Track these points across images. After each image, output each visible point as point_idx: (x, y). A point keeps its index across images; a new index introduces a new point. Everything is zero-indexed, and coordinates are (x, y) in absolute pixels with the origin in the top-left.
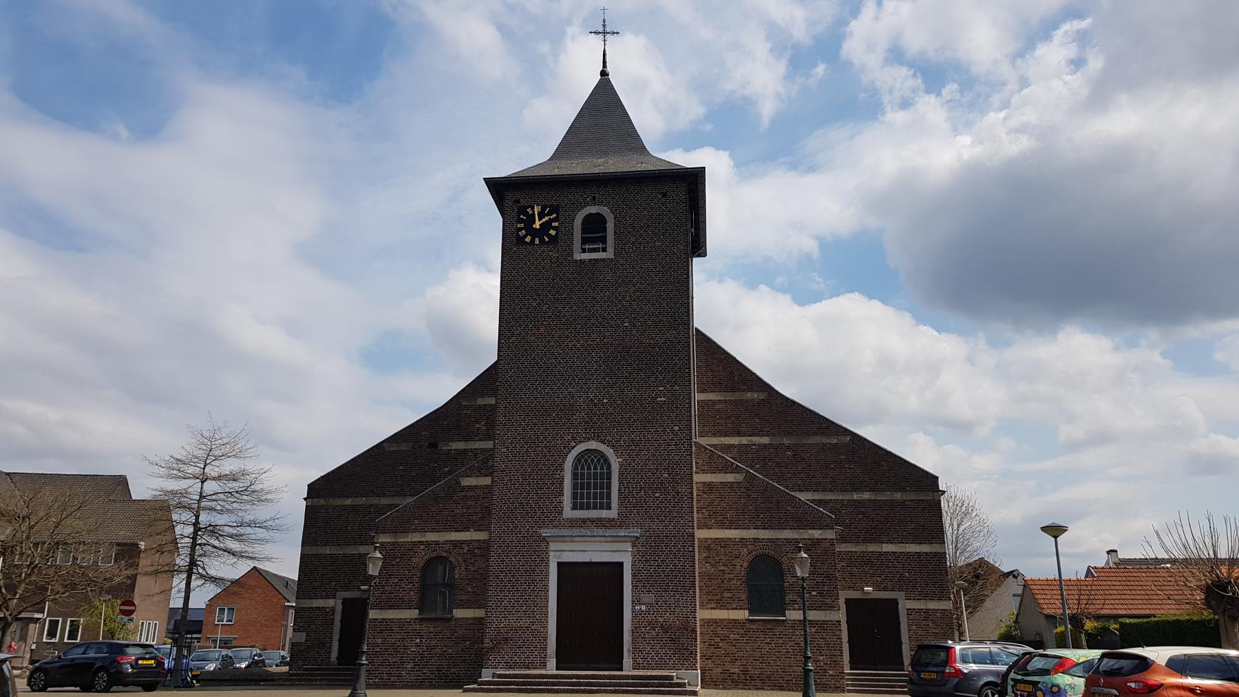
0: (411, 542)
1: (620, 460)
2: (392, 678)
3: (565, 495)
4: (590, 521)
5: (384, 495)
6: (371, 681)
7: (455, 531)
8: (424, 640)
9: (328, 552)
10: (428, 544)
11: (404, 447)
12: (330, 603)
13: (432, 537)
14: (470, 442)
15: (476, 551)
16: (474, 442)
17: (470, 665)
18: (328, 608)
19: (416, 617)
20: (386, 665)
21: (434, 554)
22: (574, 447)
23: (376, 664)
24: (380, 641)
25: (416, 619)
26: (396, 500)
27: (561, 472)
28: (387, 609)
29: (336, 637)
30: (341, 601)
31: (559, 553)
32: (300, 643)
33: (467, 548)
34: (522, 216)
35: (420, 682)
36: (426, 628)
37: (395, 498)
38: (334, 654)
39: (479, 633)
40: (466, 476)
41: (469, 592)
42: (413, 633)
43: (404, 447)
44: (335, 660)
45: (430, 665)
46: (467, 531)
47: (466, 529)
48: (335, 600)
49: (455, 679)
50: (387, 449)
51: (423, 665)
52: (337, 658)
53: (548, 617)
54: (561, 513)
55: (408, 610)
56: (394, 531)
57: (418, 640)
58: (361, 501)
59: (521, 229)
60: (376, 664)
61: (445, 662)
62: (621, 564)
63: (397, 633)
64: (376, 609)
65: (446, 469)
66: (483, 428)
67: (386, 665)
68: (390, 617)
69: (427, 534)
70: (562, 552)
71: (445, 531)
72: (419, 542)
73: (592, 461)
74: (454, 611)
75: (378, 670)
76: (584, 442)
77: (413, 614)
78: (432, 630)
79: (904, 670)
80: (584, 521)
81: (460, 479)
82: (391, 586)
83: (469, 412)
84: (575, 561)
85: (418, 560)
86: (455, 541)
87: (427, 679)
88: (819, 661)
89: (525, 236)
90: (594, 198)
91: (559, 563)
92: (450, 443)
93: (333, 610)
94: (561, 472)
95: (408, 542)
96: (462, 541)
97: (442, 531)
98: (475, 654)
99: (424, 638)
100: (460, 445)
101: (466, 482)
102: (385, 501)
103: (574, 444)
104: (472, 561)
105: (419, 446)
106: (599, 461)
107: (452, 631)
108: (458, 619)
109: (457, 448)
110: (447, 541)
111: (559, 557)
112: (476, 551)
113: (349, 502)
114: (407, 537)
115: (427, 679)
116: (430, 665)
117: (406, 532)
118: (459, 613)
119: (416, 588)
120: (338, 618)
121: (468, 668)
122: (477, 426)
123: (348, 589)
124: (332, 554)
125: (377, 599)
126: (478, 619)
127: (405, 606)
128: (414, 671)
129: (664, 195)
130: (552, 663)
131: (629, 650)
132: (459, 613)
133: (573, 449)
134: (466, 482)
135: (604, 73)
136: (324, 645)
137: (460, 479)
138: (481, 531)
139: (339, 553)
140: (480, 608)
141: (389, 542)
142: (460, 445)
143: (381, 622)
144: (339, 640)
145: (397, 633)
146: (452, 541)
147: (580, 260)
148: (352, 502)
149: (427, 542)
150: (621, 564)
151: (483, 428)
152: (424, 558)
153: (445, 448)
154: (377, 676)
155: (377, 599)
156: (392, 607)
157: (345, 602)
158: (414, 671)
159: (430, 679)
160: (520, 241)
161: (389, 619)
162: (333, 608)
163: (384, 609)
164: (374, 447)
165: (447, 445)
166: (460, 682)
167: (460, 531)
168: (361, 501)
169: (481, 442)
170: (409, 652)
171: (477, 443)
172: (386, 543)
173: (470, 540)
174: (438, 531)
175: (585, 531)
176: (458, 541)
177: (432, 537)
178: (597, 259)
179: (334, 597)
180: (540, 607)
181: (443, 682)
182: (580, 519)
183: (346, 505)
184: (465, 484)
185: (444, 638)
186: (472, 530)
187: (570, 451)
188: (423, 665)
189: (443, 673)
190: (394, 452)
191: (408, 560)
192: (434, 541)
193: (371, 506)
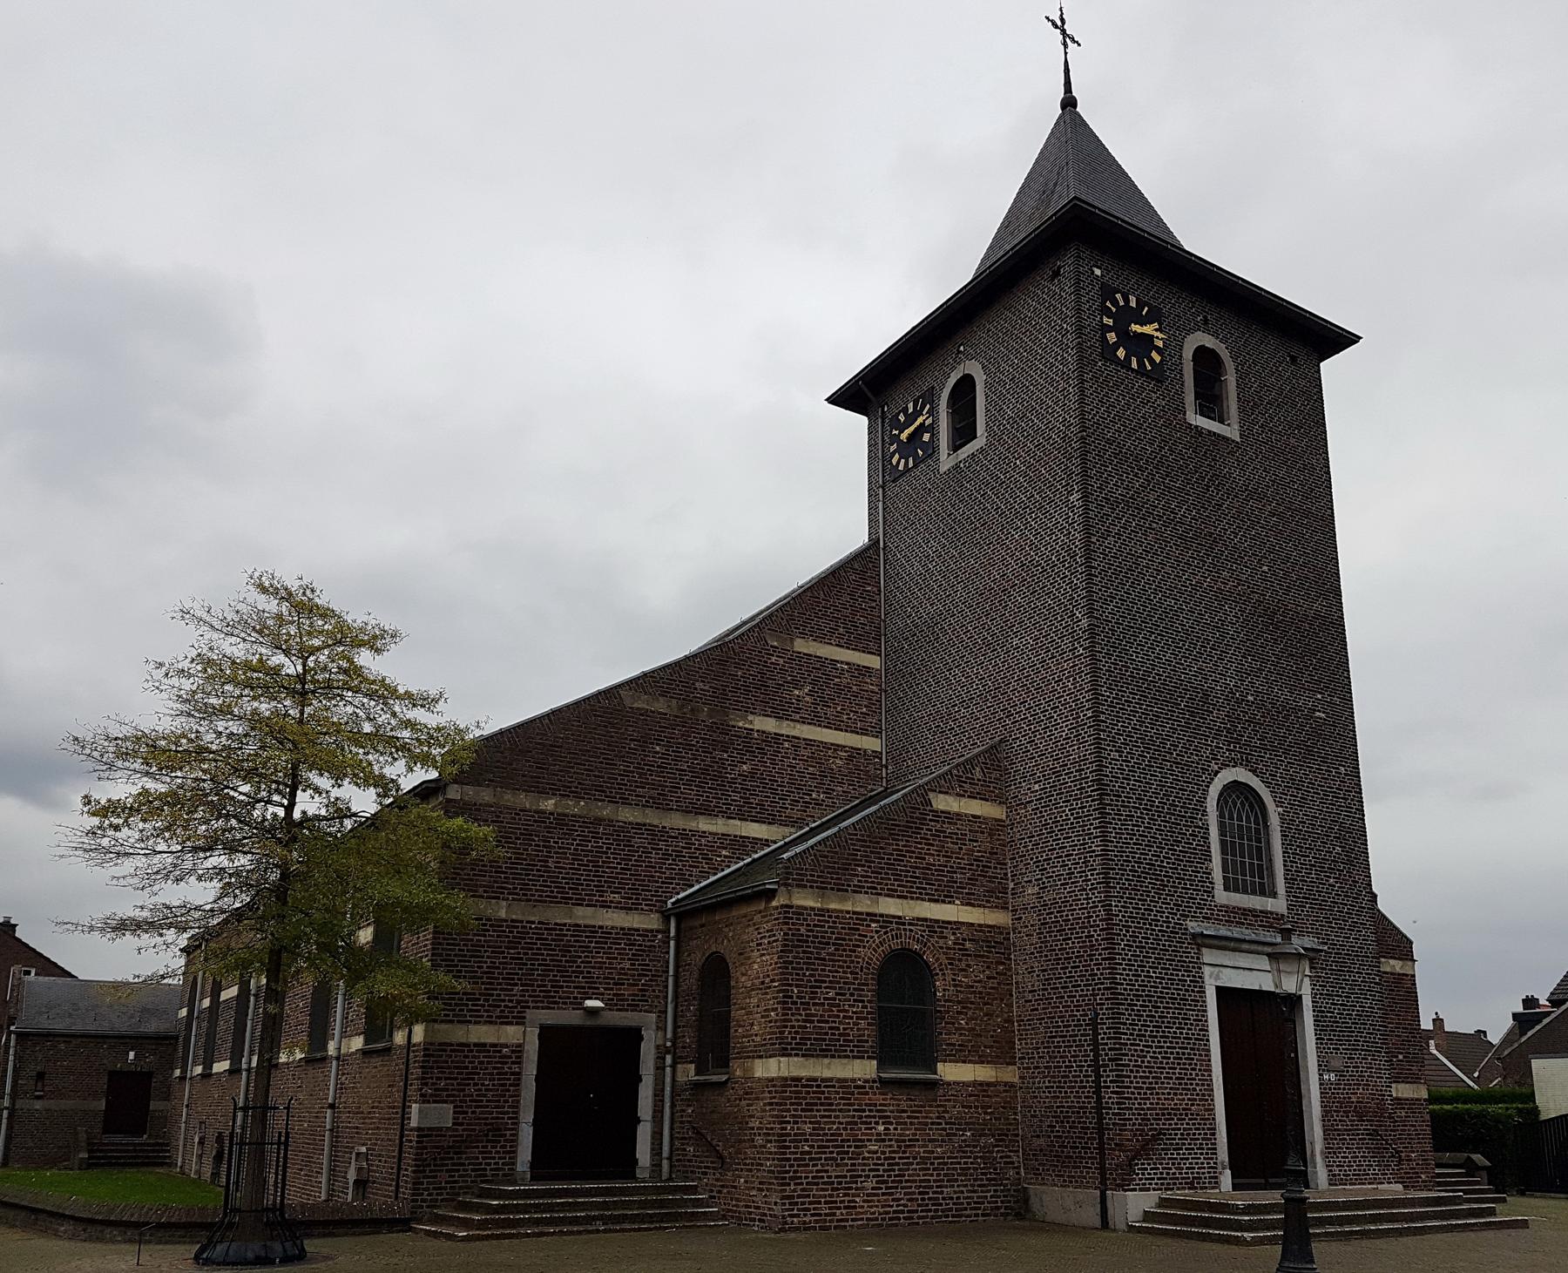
0: (854, 913)
1: (1280, 809)
2: (838, 1212)
3: (1214, 860)
4: (1253, 916)
5: (625, 802)
6: (795, 1220)
7: (930, 900)
8: (891, 1127)
9: (503, 914)
10: (886, 920)
11: (660, 706)
12: (511, 1034)
13: (890, 906)
14: (786, 723)
15: (968, 945)
16: (792, 724)
17: (975, 1180)
18: (506, 1046)
19: (874, 1076)
20: (823, 1183)
21: (896, 944)
22: (1216, 773)
23: (804, 1181)
24: (808, 1128)
25: (874, 1081)
26: (652, 818)
27: (1203, 815)
28: (818, 1056)
29: (527, 1116)
30: (537, 1031)
31: (1217, 969)
32: (440, 1129)
33: (952, 938)
34: (1108, 304)
35: (890, 1219)
36: (890, 1102)
37: (648, 811)
38: (525, 1154)
39: (986, 1113)
40: (940, 792)
41: (964, 1029)
42: (870, 1111)
43: (660, 706)
44: (526, 1168)
45: (907, 1181)
46: (950, 903)
47: (945, 898)
48: (521, 1028)
49: (951, 1210)
50: (627, 702)
51: (893, 1182)
52: (534, 1164)
53: (1212, 1090)
54: (1210, 892)
55: (858, 1061)
56: (822, 888)
57: (881, 1128)
58: (575, 807)
59: (1110, 329)
60: (804, 1181)
61: (932, 1175)
62: (1294, 1001)
63: (840, 1111)
64: (797, 1055)
65: (745, 767)
66: (807, 699)
67: (823, 1183)
68: (824, 1076)
69: (881, 899)
70: (1221, 969)
71: (912, 898)
72: (868, 914)
73: (1235, 804)
74: (734, 1064)
75: (808, 1196)
76: (1228, 766)
77: (863, 1069)
78: (904, 1105)
79: (633, 1177)
80: (1246, 912)
81: (931, 795)
82: (823, 1004)
83: (781, 661)
84: (1240, 987)
85: (870, 953)
86: (931, 920)
87: (903, 1212)
88: (1411, 1160)
89: (1116, 346)
90: (1206, 321)
91: (1218, 988)
92: (750, 717)
93: (518, 1050)
94: (1203, 815)
95: (848, 912)
96: (943, 922)
97: (906, 897)
98: (981, 1157)
99: (891, 1123)
100: (769, 725)
101: (942, 802)
102: (628, 815)
103: (1216, 767)
104: (963, 966)
105: (692, 710)
106: (1242, 804)
107: (941, 1109)
108: (949, 1084)
109: (764, 728)
110: (918, 919)
111: (1217, 978)
112: (968, 945)
113: (549, 804)
114: (845, 900)
115: (903, 1212)
116: (907, 1181)
117: (841, 889)
118: (950, 1072)
119: (868, 1013)
120: (530, 1070)
121: (972, 1186)
122: (797, 692)
123: (551, 1004)
124: (512, 921)
125: (796, 1033)
126: (981, 1084)
127: (852, 1051)
128: (877, 1195)
129: (1294, 359)
130: (1226, 1179)
131: (1322, 1152)
132: (950, 1072)
133: (1215, 775)
134: (942, 802)
135: (1069, 103)
136: (500, 1134)
137: (931, 795)
138: (973, 905)
139: (533, 919)
140: (982, 1062)
141: (813, 909)
142: (769, 725)
143: (807, 1086)
144: (535, 1124)
145: (840, 1111)
146: (925, 920)
147: (1196, 427)
148: (555, 804)
149: (882, 916)
150: (1294, 1001)
151: (807, 699)
152: (879, 951)
153: (741, 724)
154: (809, 1210)
155: (796, 1033)
156: (825, 1053)
157: (546, 1033)
158: (877, 1195)
159: (909, 1212)
160: (1108, 352)
161: (823, 1080)
162: (520, 1045)
163: (812, 1056)
164: (599, 693)
165: (745, 719)
166: (961, 1216)
167: (936, 901)
168: (575, 807)
169: (805, 727)
170: (866, 1155)
171: (798, 726)
172: (805, 908)
173: (955, 922)
174: (899, 897)
175: (1247, 932)
176: (937, 921)
177: (890, 906)
178: (1219, 435)
179: (520, 1021)
180: (1200, 1070)
181: (932, 1217)
182: (1239, 909)
183: (543, 812)
184: (941, 807)
185: (926, 1124)
186: (957, 902)
187: (1212, 779)
188: (893, 1182)
189: (930, 1199)
190: (645, 713)
191: (850, 951)
192: (894, 917)
193: (599, 821)
